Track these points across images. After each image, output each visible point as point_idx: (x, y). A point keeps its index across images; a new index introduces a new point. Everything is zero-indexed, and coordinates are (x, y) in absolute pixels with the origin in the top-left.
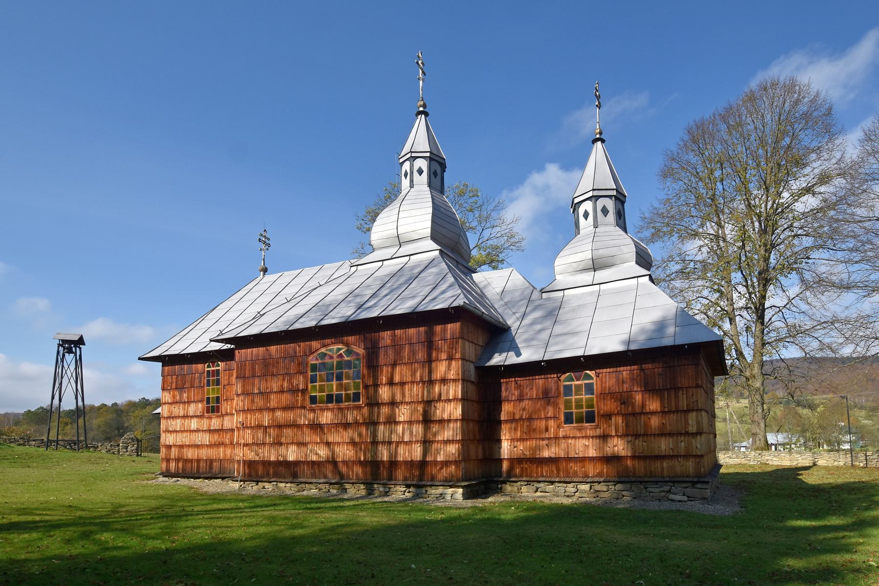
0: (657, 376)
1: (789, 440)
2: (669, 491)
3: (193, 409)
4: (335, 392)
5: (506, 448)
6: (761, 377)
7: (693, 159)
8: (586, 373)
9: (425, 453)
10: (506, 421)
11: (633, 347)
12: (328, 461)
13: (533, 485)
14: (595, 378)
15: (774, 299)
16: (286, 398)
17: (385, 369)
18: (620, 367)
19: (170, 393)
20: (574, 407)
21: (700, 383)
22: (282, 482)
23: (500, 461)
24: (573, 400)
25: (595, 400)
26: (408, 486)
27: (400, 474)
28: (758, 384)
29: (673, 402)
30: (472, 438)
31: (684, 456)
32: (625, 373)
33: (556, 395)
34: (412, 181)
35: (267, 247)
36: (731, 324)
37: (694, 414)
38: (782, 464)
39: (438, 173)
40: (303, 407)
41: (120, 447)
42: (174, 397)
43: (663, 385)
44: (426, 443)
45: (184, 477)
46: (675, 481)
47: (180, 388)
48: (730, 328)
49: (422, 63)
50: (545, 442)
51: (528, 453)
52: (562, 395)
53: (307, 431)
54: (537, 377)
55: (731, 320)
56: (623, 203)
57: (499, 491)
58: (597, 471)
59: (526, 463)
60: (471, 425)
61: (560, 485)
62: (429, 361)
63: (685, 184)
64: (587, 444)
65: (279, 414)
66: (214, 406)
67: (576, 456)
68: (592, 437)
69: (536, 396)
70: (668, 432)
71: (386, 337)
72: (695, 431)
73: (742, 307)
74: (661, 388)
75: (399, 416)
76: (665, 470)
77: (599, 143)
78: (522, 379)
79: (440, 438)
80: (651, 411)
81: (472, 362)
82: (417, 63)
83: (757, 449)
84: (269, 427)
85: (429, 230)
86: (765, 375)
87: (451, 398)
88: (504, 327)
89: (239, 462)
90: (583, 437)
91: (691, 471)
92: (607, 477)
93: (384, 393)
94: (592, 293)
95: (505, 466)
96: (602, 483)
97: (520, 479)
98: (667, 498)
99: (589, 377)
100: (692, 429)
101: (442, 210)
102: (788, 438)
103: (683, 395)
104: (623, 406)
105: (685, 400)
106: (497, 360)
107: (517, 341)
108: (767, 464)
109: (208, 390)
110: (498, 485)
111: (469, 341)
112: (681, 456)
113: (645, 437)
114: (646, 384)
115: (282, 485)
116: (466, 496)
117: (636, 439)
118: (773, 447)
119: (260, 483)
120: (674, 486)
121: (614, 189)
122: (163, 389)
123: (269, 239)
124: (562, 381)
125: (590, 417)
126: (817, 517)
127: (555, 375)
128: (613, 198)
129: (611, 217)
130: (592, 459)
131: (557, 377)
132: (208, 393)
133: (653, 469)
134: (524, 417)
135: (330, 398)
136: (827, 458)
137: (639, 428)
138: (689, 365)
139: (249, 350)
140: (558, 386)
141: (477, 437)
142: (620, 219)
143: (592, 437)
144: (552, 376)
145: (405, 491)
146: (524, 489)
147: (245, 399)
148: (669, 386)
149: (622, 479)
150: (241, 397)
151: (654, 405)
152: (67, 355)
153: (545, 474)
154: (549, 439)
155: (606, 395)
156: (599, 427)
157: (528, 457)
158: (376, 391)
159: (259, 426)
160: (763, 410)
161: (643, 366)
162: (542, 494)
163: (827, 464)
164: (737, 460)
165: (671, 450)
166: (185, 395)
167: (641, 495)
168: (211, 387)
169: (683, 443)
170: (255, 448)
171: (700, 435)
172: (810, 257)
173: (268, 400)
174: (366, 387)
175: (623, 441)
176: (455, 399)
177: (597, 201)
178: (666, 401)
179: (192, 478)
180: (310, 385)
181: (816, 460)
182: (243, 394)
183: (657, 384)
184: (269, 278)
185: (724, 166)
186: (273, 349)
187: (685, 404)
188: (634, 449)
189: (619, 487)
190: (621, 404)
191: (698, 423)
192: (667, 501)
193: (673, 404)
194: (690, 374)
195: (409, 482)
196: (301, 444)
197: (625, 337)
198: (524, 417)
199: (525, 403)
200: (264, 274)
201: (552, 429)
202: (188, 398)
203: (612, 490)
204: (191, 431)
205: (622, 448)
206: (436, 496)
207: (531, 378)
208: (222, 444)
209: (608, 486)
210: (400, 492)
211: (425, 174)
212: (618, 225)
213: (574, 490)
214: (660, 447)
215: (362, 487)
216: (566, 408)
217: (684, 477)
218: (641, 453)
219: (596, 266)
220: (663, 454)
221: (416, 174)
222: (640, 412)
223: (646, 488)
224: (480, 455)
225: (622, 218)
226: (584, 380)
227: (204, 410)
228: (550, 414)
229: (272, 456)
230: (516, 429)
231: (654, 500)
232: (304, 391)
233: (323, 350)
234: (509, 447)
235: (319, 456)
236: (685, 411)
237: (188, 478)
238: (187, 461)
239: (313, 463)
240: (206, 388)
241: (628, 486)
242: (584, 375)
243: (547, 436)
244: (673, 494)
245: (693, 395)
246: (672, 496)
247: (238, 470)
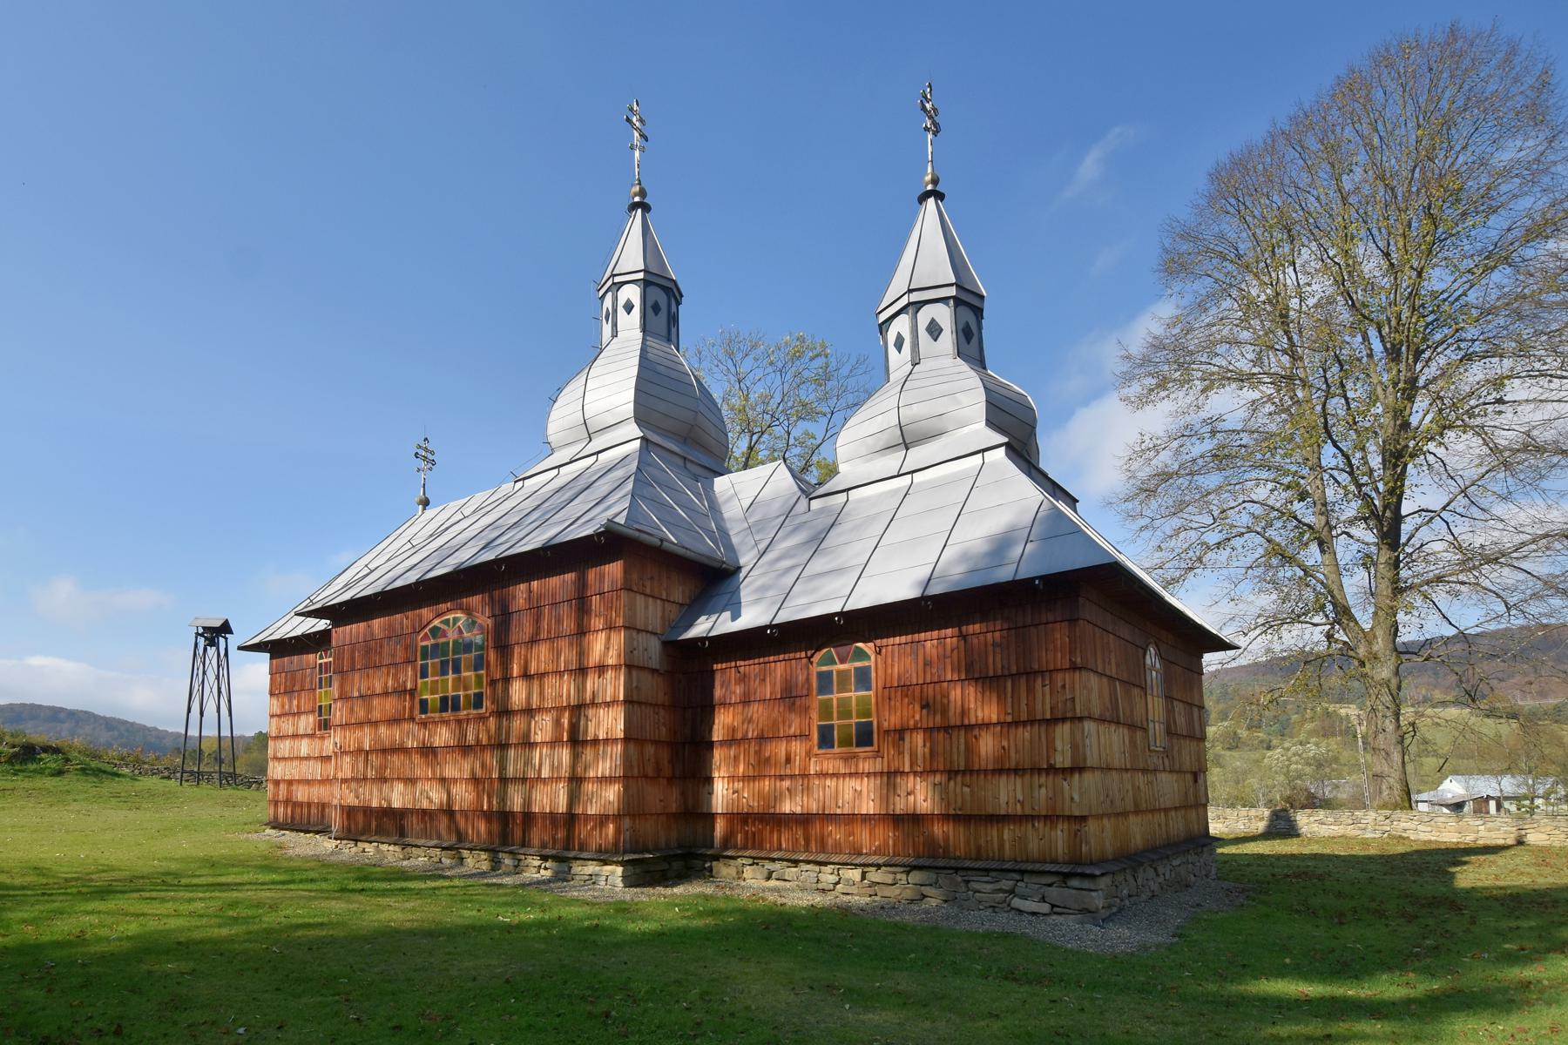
0: (990, 648)
1: (1529, 790)
2: (1012, 892)
4: (451, 693)
5: (722, 794)
6: (1393, 659)
7: (1230, 227)
8: (857, 647)
9: (573, 798)
10: (723, 743)
11: (936, 589)
12: (441, 810)
13: (763, 866)
14: (873, 658)
15: (1421, 493)
16: (389, 706)
17: (517, 650)
18: (919, 632)
20: (854, 714)
21: (1079, 660)
22: (383, 843)
23: (711, 817)
24: (835, 702)
25: (873, 700)
26: (544, 858)
27: (536, 836)
28: (1384, 672)
29: (1024, 701)
30: (650, 773)
31: (1045, 817)
32: (928, 644)
33: (805, 692)
34: (615, 325)
35: (430, 465)
36: (1323, 551)
37: (1067, 726)
38: (1439, 839)
40: (412, 719)
43: (1003, 667)
44: (576, 781)
45: (292, 830)
46: (1023, 869)
47: (289, 692)
48: (1320, 560)
49: (641, 120)
50: (786, 783)
51: (756, 804)
52: (815, 692)
53: (416, 758)
54: (772, 658)
55: (1321, 544)
57: (708, 874)
58: (877, 843)
60: (650, 750)
61: (810, 867)
62: (582, 632)
63: (1216, 281)
64: (859, 788)
65: (383, 730)
67: (839, 811)
68: (868, 775)
69: (771, 694)
70: (1013, 765)
71: (520, 593)
72: (1067, 764)
73: (1356, 518)
74: (999, 673)
75: (535, 733)
76: (1007, 846)
77: (931, 201)
78: (747, 663)
79: (592, 774)
80: (980, 722)
81: (655, 634)
82: (628, 120)
83: (1384, 806)
84: (371, 751)
85: (631, 406)
86: (1401, 653)
88: (724, 566)
89: (336, 806)
90: (851, 775)
91: (1060, 851)
92: (894, 856)
93: (518, 693)
94: (894, 492)
95: (720, 828)
96: (883, 868)
97: (740, 854)
98: (1009, 905)
99: (861, 655)
100: (1062, 759)
101: (661, 369)
102: (1527, 785)
103: (1044, 686)
104: (925, 711)
105: (1048, 697)
106: (702, 627)
107: (743, 594)
108: (1404, 838)
109: (320, 693)
110: (705, 862)
111: (646, 595)
112: (1039, 817)
113: (968, 778)
114: (969, 667)
115: (384, 847)
116: (629, 881)
117: (949, 779)
118: (1492, 804)
119: (359, 843)
120: (1022, 881)
121: (951, 285)
122: (272, 694)
123: (432, 453)
124: (815, 665)
125: (864, 736)
127: (803, 654)
128: (952, 302)
129: (947, 339)
130: (866, 818)
131: (806, 657)
133: (982, 842)
134: (750, 736)
135: (444, 704)
136: (1549, 828)
137: (955, 757)
138: (1055, 622)
139: (348, 627)
140: (808, 674)
141: (667, 772)
143: (868, 775)
144: (798, 655)
145: (540, 866)
146: (748, 872)
148: (1014, 670)
149: (921, 862)
151: (985, 710)
152: (209, 648)
153: (784, 846)
154: (792, 777)
155: (893, 690)
156: (880, 754)
157: (756, 811)
158: (506, 690)
159: (360, 750)
160: (1399, 727)
161: (964, 628)
162: (778, 883)
163: (1548, 842)
164: (1336, 828)
165: (1018, 805)
167: (957, 895)
168: (323, 690)
169: (1043, 791)
170: (353, 785)
171: (1080, 773)
172: (1506, 399)
173: (369, 710)
174: (493, 683)
175: (924, 784)
176: (614, 702)
177: (917, 312)
178: (1009, 700)
179: (302, 831)
180: (419, 681)
181: (1523, 832)
182: (341, 698)
183: (991, 667)
184: (430, 513)
185: (1294, 232)
186: (377, 624)
187: (1048, 706)
188: (945, 798)
189: (916, 877)
190: (922, 707)
191: (1075, 747)
192: (1008, 912)
193: (1024, 707)
194: (1059, 642)
195: (548, 852)
196: (411, 781)
197: (925, 572)
198: (750, 736)
199: (756, 710)
200: (424, 509)
201: (798, 758)
202: (298, 706)
203: (903, 882)
204: (301, 759)
205: (923, 798)
206: (582, 877)
207: (762, 660)
209: (895, 873)
210: (537, 870)
211: (636, 311)
213: (834, 878)
214: (996, 797)
215: (484, 856)
217: (1046, 863)
218: (960, 810)
219: (907, 440)
220: (1003, 812)
221: (621, 311)
222: (958, 723)
223: (967, 882)
224: (674, 805)
228: (793, 729)
229: (374, 798)
230: (736, 759)
231: (981, 907)
232: (412, 692)
233: (436, 622)
234: (725, 792)
235: (431, 801)
237: (298, 831)
238: (297, 805)
239: (424, 812)
240: (318, 690)
241: (932, 875)
242: (855, 652)
243: (788, 772)
245: (1064, 686)
246: (1017, 902)
247: (336, 820)
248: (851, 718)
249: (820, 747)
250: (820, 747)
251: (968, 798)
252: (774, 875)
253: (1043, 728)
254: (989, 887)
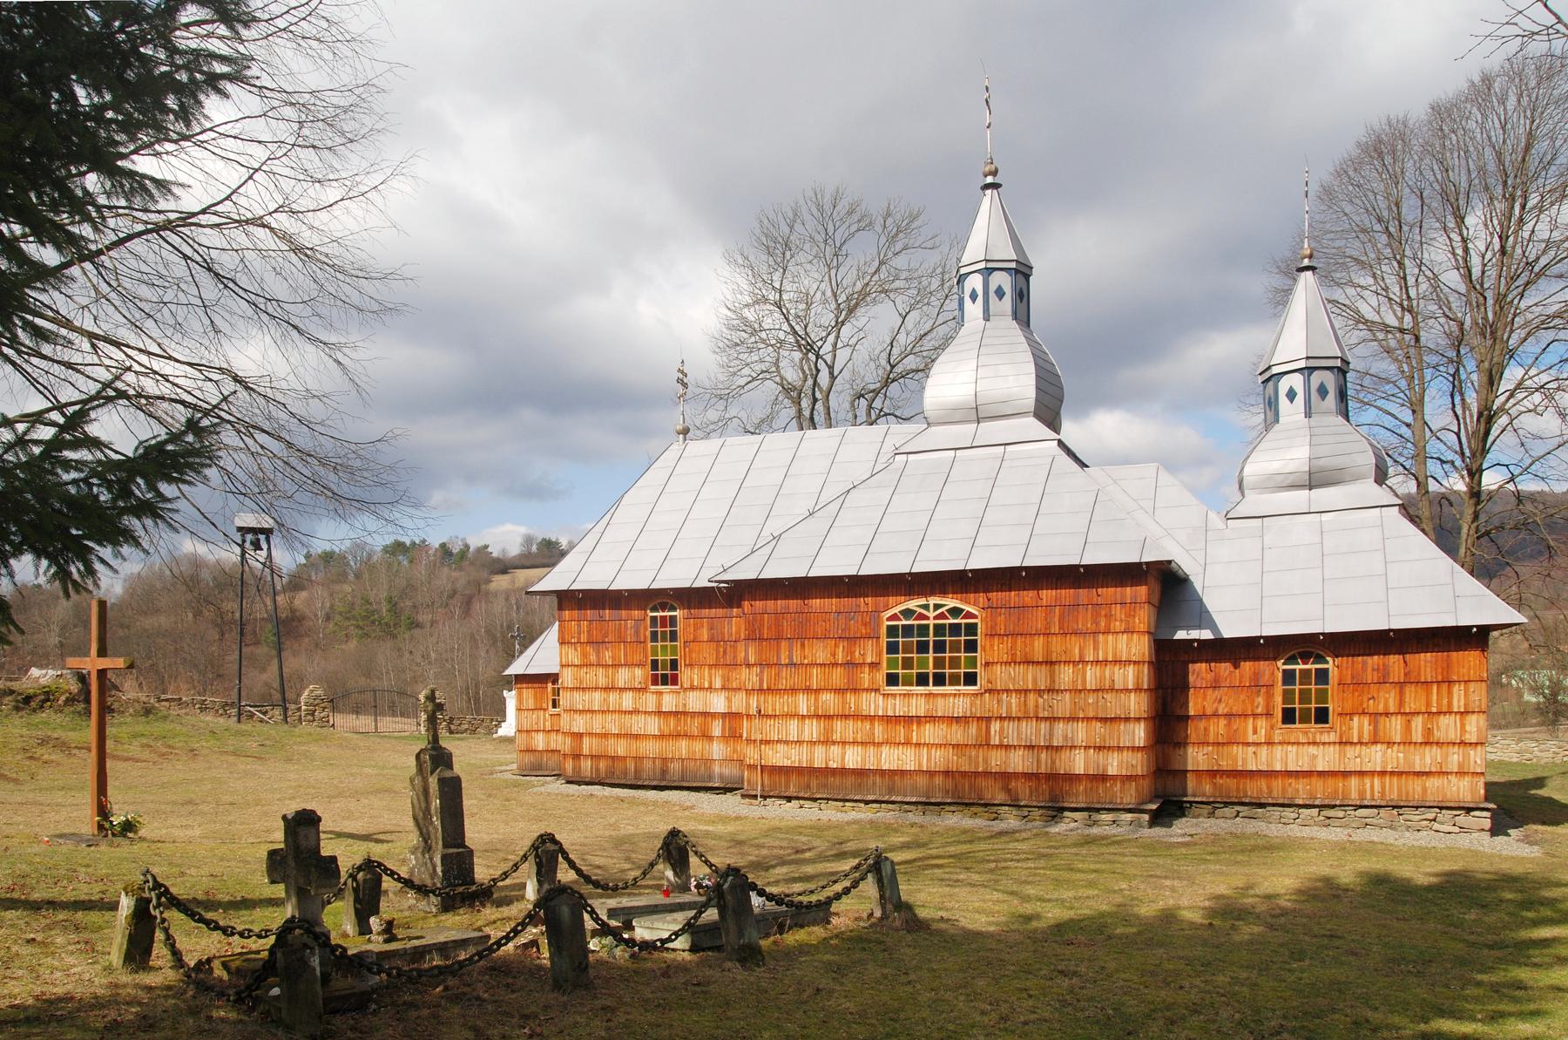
3: (623, 676)
19: (576, 650)
39: (1317, 394)
41: (303, 714)
42: (584, 655)
56: (1027, 277)
59: (1221, 777)
66: (667, 675)
87: (1130, 687)
112: (1451, 773)
113: (1402, 746)
121: (1013, 261)
132: (655, 652)
142: (1021, 301)
147: (762, 672)
148: (1440, 679)
150: (756, 670)
166: (608, 654)
168: (659, 644)
169: (1456, 756)
193: (1445, 701)
208: (677, 736)
211: (1008, 299)
212: (1015, 317)
225: (1025, 299)
236: (1462, 713)
244: (1439, 823)
248: (903, 658)
249: (1283, 723)
250: (1283, 723)
251: (1402, 761)
252: (1241, 815)
253: (1458, 717)
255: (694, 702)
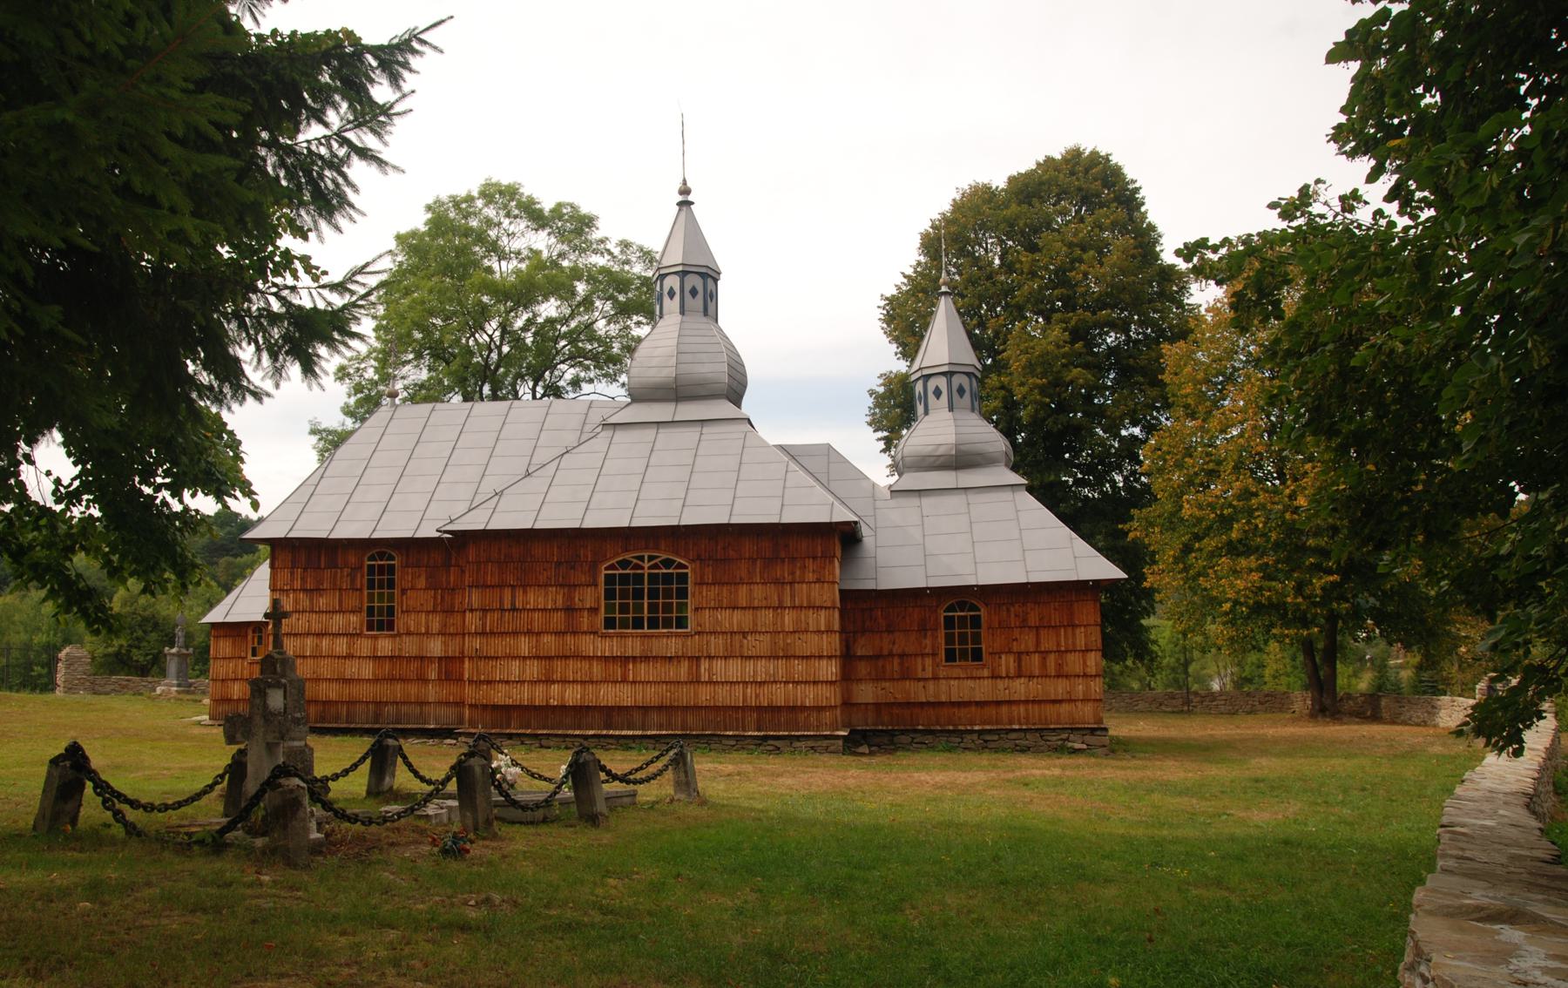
2: (1067, 739)
3: (338, 622)
72: (1094, 673)
87: (823, 629)
126: (896, 750)
216: (946, 644)
226: (969, 611)
227: (361, 625)
251: (1040, 691)
254: (1055, 738)
255: (409, 646)
